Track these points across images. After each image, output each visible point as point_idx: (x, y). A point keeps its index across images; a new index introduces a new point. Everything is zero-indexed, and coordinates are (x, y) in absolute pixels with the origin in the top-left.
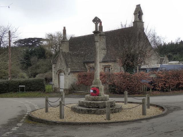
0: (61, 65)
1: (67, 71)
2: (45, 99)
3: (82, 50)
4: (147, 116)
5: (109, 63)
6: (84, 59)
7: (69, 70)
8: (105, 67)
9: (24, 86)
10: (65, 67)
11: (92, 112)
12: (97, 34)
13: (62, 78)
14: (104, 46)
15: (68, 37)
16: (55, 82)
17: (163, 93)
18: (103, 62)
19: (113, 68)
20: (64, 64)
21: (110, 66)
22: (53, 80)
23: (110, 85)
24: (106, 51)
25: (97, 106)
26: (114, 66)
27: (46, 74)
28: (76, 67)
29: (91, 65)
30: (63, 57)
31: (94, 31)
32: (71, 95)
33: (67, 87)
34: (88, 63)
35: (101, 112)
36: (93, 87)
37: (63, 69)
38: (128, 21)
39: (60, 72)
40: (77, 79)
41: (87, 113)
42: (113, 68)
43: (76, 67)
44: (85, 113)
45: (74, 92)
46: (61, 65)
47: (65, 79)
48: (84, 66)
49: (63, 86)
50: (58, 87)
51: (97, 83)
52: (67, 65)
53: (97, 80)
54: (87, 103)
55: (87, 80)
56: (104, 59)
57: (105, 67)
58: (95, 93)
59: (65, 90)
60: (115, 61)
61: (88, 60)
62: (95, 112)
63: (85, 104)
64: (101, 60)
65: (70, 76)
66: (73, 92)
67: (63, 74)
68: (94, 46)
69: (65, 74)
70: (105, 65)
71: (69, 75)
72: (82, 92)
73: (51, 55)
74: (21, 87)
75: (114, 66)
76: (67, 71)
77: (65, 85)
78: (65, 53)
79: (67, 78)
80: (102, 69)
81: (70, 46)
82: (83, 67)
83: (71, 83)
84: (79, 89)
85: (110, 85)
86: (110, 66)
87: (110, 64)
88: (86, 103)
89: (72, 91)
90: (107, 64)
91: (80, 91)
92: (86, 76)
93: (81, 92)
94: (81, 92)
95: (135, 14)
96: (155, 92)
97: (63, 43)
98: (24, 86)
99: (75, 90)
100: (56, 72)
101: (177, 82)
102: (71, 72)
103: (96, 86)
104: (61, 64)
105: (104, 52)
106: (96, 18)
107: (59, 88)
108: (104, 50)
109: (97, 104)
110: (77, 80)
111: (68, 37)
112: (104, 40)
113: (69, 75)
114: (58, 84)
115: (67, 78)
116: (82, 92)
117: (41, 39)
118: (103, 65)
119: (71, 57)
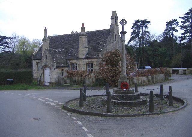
0: (46, 61)
2: (79, 91)
4: (84, 109)
5: (92, 60)
7: (55, 66)
9: (12, 80)
13: (47, 72)
14: (86, 44)
18: (86, 58)
21: (93, 62)
24: (88, 48)
29: (74, 61)
31: (28, 42)
33: (54, 80)
34: (70, 59)
37: (49, 64)
38: (106, 25)
48: (67, 62)
53: (124, 75)
56: (86, 56)
69: (51, 69)
71: (55, 69)
74: (9, 81)
80: (85, 64)
87: (93, 60)
89: (57, 85)
90: (90, 60)
95: (112, 19)
97: (45, 41)
98: (12, 80)
105: (87, 50)
106: (115, 12)
117: (6, 37)
118: (86, 61)
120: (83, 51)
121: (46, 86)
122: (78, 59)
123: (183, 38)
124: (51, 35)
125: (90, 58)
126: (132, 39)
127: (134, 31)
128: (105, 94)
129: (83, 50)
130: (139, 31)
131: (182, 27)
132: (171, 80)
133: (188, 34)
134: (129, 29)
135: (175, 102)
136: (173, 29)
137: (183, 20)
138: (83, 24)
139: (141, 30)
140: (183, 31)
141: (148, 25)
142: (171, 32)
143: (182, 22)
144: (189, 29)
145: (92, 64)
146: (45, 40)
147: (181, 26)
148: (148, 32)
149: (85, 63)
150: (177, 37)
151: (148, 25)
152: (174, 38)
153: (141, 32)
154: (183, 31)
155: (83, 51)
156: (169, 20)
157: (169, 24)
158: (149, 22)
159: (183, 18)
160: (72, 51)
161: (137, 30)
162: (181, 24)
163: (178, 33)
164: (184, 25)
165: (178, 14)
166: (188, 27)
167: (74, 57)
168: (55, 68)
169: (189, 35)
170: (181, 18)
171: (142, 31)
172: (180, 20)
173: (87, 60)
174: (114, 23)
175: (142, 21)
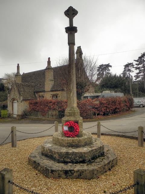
0: (14, 94)
1: (20, 99)
3: (32, 82)
5: (57, 92)
6: (34, 89)
8: (53, 96)
10: (18, 96)
11: (75, 174)
12: (72, 32)
13: (15, 105)
15: (21, 73)
16: (9, 108)
17: (105, 117)
18: (52, 91)
19: (60, 96)
20: (17, 93)
21: (58, 94)
22: (8, 107)
23: (59, 111)
25: (81, 159)
26: (62, 94)
27: (4, 102)
28: (27, 96)
29: (41, 94)
30: (16, 86)
32: (23, 120)
33: (20, 113)
35: (93, 174)
36: (67, 121)
37: (16, 97)
39: (13, 100)
40: (28, 106)
41: (64, 176)
42: (60, 96)
43: (27, 96)
44: (60, 177)
45: (26, 118)
46: (14, 94)
47: (18, 106)
49: (16, 112)
50: (12, 113)
51: (75, 113)
52: (20, 94)
53: (73, 108)
54: (60, 154)
55: (38, 107)
56: (52, 88)
57: (53, 96)
58: (71, 131)
59: (18, 115)
60: (63, 90)
61: (37, 90)
62: (81, 175)
63: (56, 156)
64: (50, 89)
65: (22, 103)
66: (25, 117)
67: (16, 101)
68: (44, 77)
69: (18, 102)
70: (53, 93)
71: (21, 102)
72: (33, 117)
73: (8, 89)
75: (62, 94)
76: (20, 99)
77: (18, 111)
78: (18, 84)
79: (19, 105)
81: (22, 80)
82: (33, 96)
83: (24, 109)
84: (30, 115)
85: (59, 111)
86: (58, 94)
88: (58, 153)
90: (55, 93)
91: (31, 117)
92: (37, 103)
93: (32, 117)
94: (32, 117)
96: (99, 116)
99: (26, 115)
100: (10, 100)
101: (114, 107)
102: (23, 100)
103: (72, 119)
104: (14, 94)
105: (53, 83)
107: (13, 113)
108: (52, 81)
109: (81, 155)
110: (28, 107)
111: (21, 73)
112: (52, 73)
113: (21, 102)
114: (12, 111)
115: (19, 105)
116: (33, 117)
118: (52, 94)
119: (23, 87)
120: (49, 85)
121: (14, 118)
122: (44, 91)
123: (137, 77)
124: (26, 72)
125: (55, 91)
126: (98, 79)
127: (100, 73)
128: (18, 142)
129: (49, 83)
130: (103, 73)
131: (137, 68)
132: (132, 111)
133: (142, 74)
134: (96, 72)
135: (136, 135)
136: (129, 70)
137: (138, 63)
138: (49, 58)
139: (105, 72)
140: (138, 71)
141: (110, 68)
142: (128, 72)
143: (136, 64)
144: (142, 70)
145: (57, 96)
146: (17, 75)
147: (136, 67)
148: (110, 73)
149: (50, 95)
150: (83, 153)
151: (110, 68)
152: (130, 77)
153: (105, 74)
154: (138, 71)
155: (49, 85)
156: (126, 63)
157: (127, 66)
158: (111, 66)
159: (137, 61)
160: (40, 84)
161: (101, 72)
162: (135, 66)
163: (133, 73)
164: (138, 66)
165: (132, 57)
166: (141, 68)
167: (41, 90)
168: (22, 101)
169: (142, 74)
170: (136, 61)
171: (106, 73)
172: (135, 63)
173: (52, 92)
174: (79, 57)
175: (105, 65)
